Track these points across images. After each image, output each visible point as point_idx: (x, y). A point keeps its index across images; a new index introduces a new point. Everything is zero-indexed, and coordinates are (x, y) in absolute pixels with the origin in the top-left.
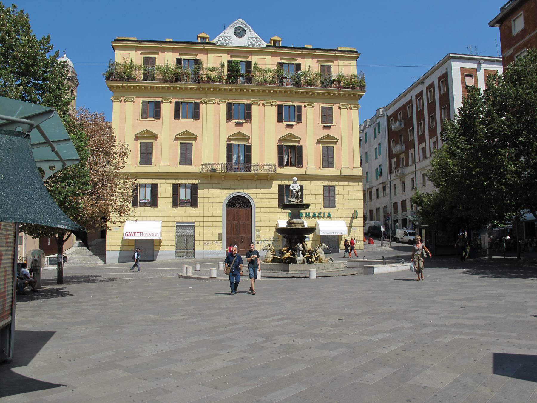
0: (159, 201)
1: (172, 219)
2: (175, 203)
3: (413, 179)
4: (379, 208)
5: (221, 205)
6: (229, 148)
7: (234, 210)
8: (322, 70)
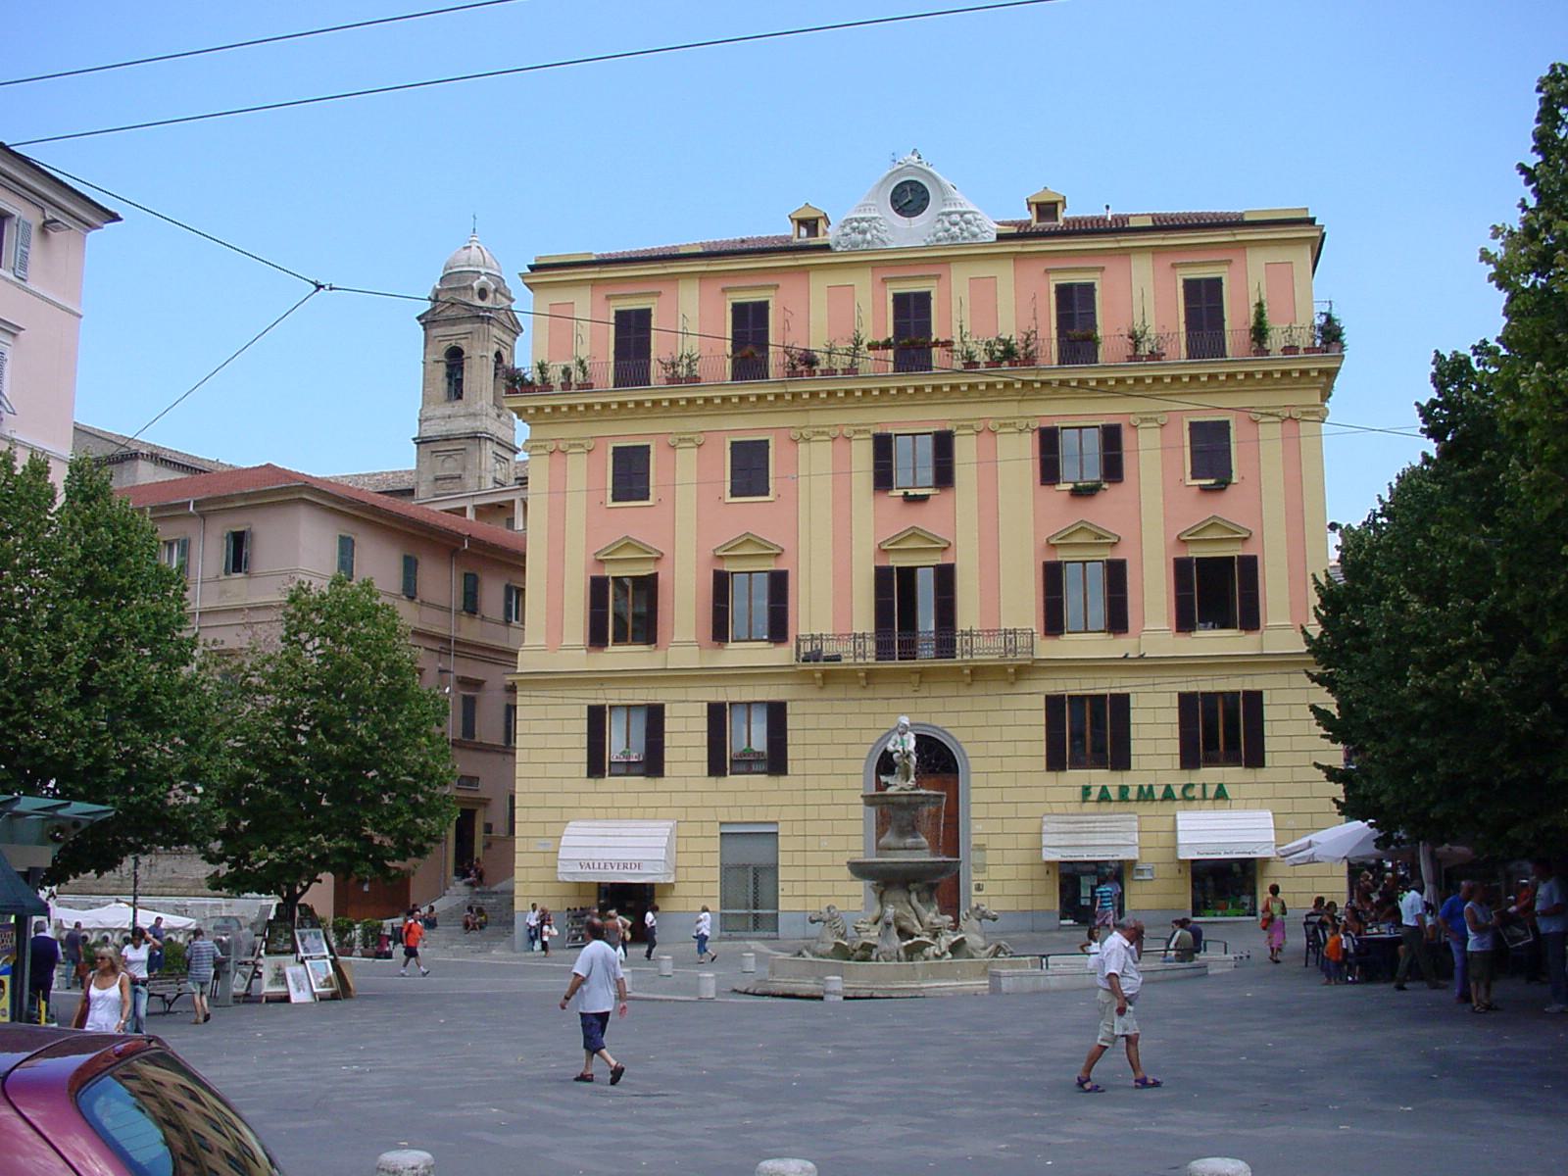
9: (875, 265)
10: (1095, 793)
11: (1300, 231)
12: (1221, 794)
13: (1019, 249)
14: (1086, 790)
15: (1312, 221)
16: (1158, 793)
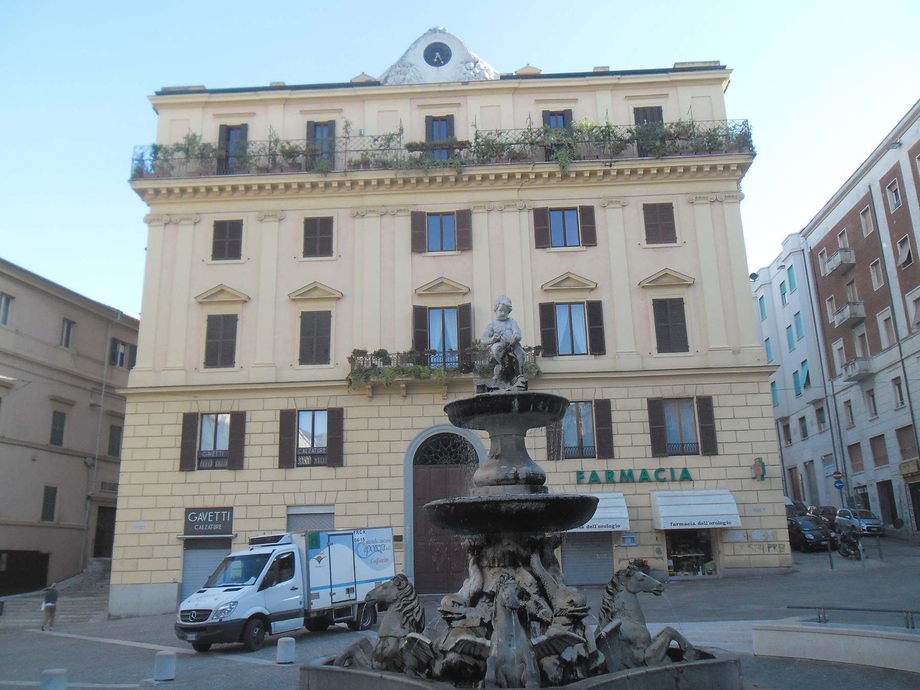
0: (179, 450)
1: (177, 502)
2: (288, 456)
3: (897, 381)
4: (812, 462)
5: (401, 459)
6: (421, 317)
7: (434, 471)
8: (637, 121)
9: (411, 96)
10: (587, 476)
11: (712, 73)
12: (686, 476)
13: (516, 85)
14: (580, 475)
15: (724, 67)
16: (637, 475)
